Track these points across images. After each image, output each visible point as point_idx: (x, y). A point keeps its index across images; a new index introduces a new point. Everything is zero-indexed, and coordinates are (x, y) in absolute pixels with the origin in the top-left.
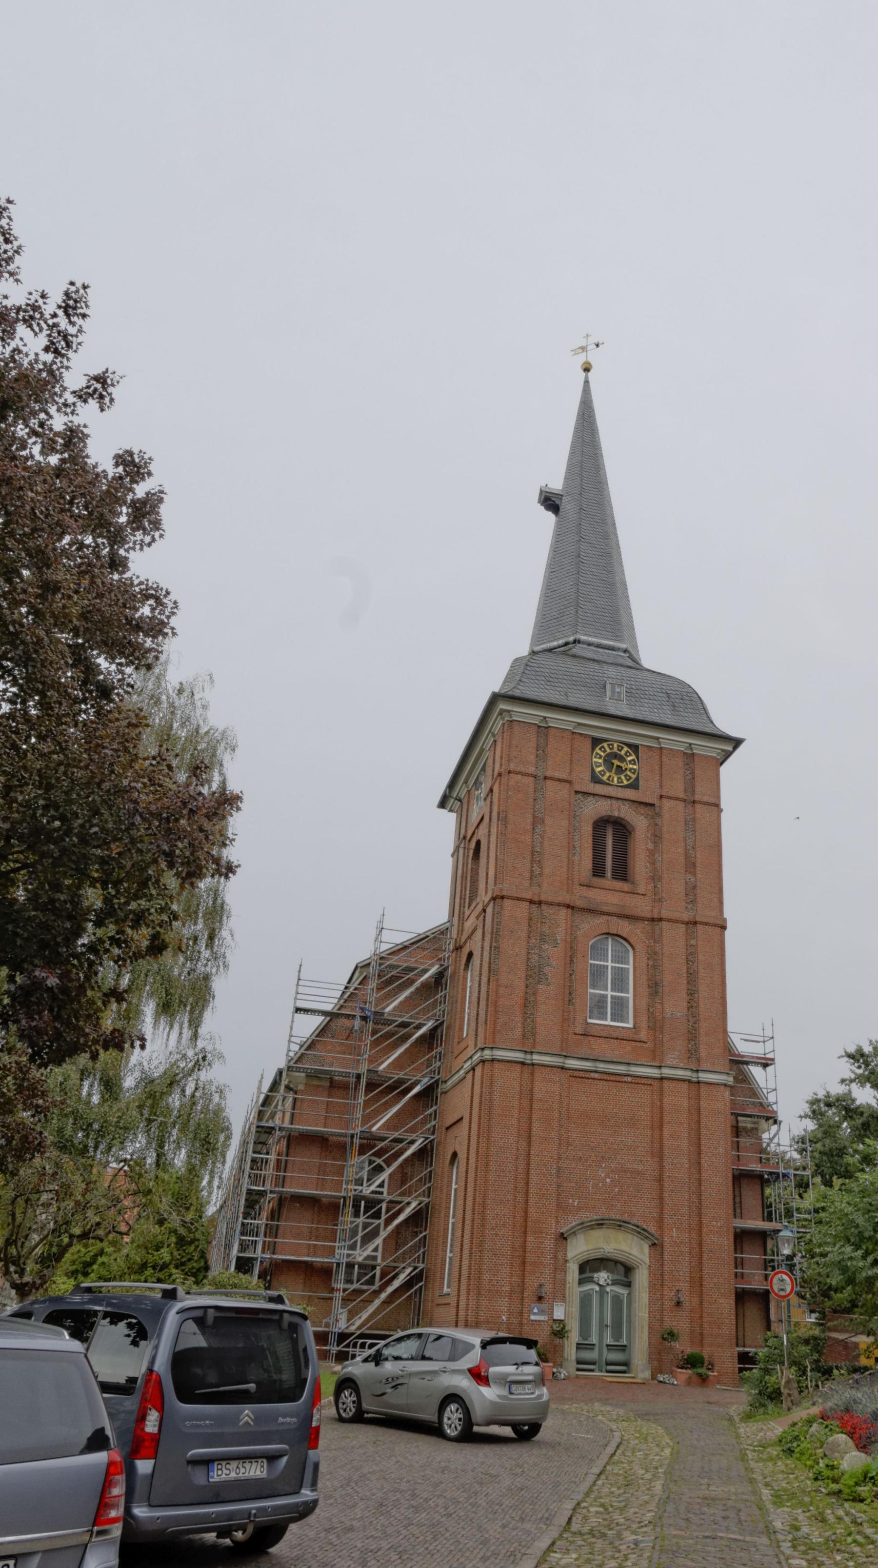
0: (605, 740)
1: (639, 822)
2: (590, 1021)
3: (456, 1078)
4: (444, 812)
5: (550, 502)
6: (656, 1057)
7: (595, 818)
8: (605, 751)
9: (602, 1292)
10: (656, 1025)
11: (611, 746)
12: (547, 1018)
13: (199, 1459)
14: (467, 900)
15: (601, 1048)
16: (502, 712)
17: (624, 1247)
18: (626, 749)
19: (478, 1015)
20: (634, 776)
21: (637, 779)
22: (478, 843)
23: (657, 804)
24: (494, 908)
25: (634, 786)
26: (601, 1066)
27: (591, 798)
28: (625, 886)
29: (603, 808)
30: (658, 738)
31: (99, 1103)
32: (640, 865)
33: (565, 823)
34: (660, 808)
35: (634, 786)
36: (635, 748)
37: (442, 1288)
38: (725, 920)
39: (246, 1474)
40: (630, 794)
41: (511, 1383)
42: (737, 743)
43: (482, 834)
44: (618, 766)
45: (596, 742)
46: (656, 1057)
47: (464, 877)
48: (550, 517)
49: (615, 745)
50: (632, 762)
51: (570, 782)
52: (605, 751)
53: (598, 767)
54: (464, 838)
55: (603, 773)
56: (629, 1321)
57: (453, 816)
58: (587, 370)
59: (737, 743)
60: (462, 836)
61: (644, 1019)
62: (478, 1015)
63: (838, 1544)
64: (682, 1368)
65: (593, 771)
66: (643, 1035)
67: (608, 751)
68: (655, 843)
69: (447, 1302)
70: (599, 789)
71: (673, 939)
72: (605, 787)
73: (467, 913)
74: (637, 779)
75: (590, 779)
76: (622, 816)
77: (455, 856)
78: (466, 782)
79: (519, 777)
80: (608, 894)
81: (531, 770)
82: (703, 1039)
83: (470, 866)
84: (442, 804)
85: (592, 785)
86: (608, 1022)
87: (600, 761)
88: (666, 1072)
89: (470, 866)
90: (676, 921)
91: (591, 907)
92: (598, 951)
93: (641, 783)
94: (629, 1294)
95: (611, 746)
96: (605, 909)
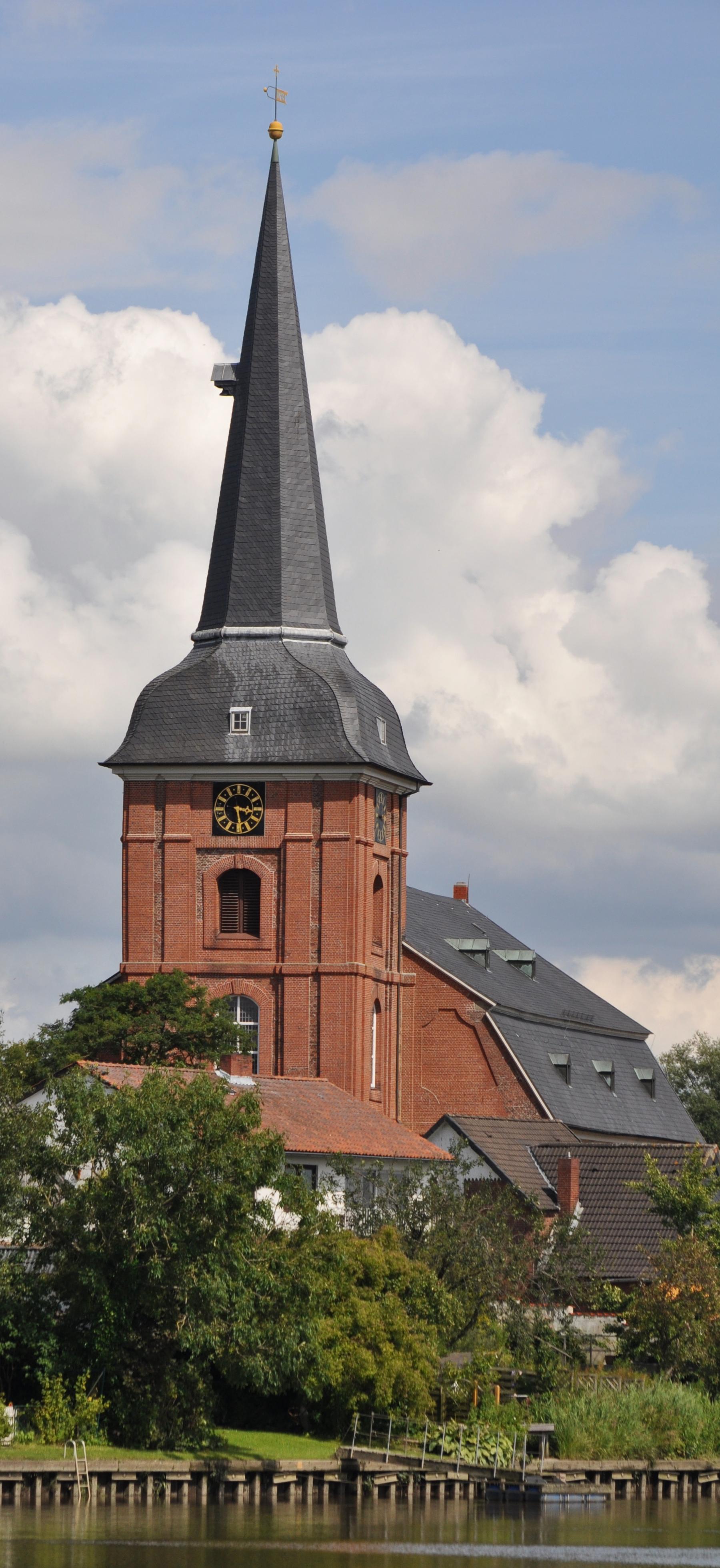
1: (267, 870)
7: (219, 873)
8: (243, 792)
13: (281, 243)
29: (225, 862)
39: (150, 1520)
40: (254, 842)
44: (241, 812)
50: (244, 828)
52: (243, 792)
53: (220, 816)
55: (225, 823)
63: (49, 1392)
69: (501, 1079)
70: (222, 842)
72: (227, 838)
74: (262, 822)
75: (210, 832)
79: (138, 845)
85: (214, 838)
87: (222, 809)
91: (215, 970)
96: (229, 970)
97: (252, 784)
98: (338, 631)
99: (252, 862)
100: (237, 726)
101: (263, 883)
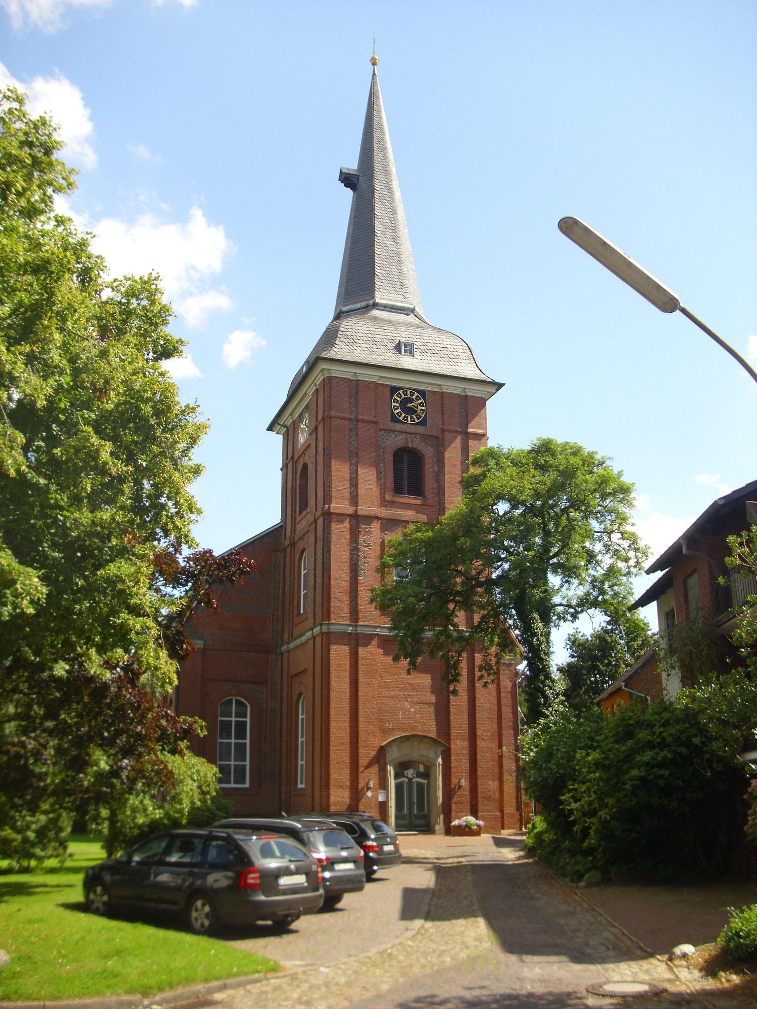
0: (400, 389)
1: (428, 452)
3: (298, 642)
4: (272, 434)
5: (348, 180)
9: (410, 780)
11: (421, 404)
14: (298, 508)
16: (323, 370)
17: (424, 753)
18: (416, 394)
19: (315, 598)
22: (305, 466)
24: (324, 521)
25: (423, 423)
33: (373, 455)
34: (443, 439)
35: (423, 423)
36: (423, 393)
37: (296, 785)
40: (421, 429)
41: (62, 499)
42: (500, 386)
43: (309, 459)
45: (394, 390)
47: (294, 490)
48: (349, 193)
51: (376, 423)
54: (293, 458)
55: (399, 414)
56: (428, 796)
57: (281, 437)
58: (374, 64)
59: (500, 386)
60: (290, 456)
62: (315, 598)
68: (438, 466)
70: (398, 427)
73: (298, 518)
76: (415, 446)
77: (285, 471)
78: (291, 414)
81: (347, 415)
83: (298, 482)
84: (270, 428)
85: (392, 424)
87: (398, 405)
89: (298, 482)
94: (428, 784)
95: (412, 419)
97: (418, 391)
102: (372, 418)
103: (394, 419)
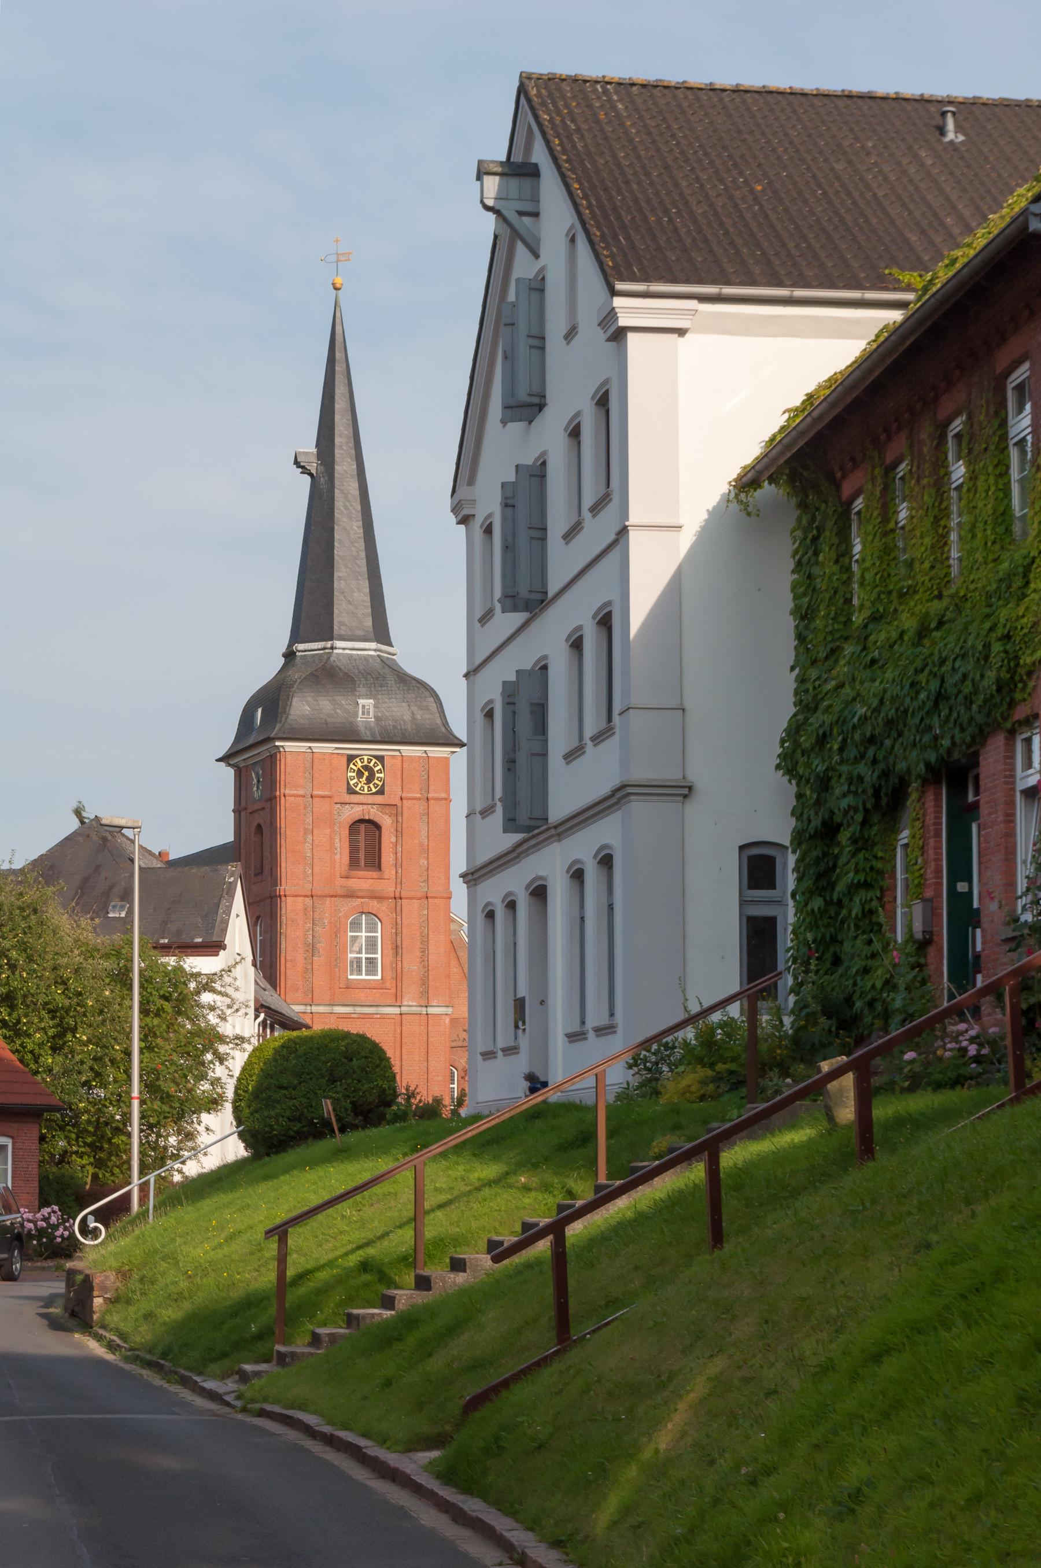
1: (386, 822)
2: (350, 977)
6: (397, 999)
10: (398, 977)
11: (379, 771)
12: (320, 979)
15: (361, 995)
20: (380, 784)
21: (383, 785)
23: (399, 805)
25: (381, 792)
26: (359, 1010)
27: (347, 806)
28: (375, 874)
29: (354, 812)
30: (399, 750)
31: (465, 1119)
32: (387, 857)
35: (381, 792)
38: (451, 893)
40: (379, 799)
46: (397, 999)
49: (350, 774)
61: (389, 974)
64: (597, 1175)
65: (348, 783)
66: (388, 985)
67: (376, 781)
70: (354, 798)
71: (411, 909)
80: (364, 881)
82: (431, 983)
86: (364, 977)
87: (354, 774)
88: (404, 1009)
90: (412, 898)
92: (356, 926)
93: (386, 789)
95: (379, 771)
96: (360, 894)
97: (376, 757)
98: (390, 645)
99: (374, 814)
100: (363, 713)
101: (383, 830)
102: (327, 793)
103: (351, 791)
